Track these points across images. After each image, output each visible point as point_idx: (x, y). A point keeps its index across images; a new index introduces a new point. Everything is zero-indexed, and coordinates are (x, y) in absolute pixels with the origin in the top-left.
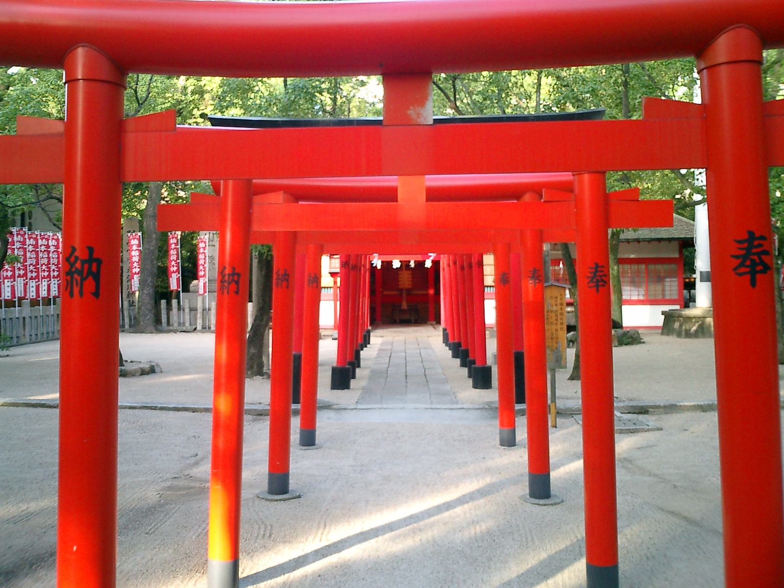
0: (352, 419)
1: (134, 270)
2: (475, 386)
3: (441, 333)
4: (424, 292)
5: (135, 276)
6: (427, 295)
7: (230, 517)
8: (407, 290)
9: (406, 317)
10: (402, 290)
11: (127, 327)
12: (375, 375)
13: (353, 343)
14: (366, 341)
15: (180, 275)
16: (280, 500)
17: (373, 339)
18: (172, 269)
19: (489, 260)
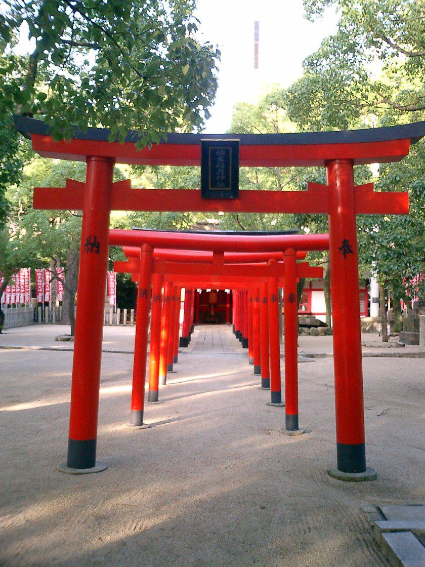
0: (190, 356)
1: (60, 289)
2: (244, 347)
3: (232, 328)
4: (223, 306)
5: (60, 292)
6: (226, 307)
7: (110, 383)
8: (214, 304)
9: (212, 320)
10: (211, 304)
11: (54, 321)
12: (197, 343)
13: (189, 331)
14: (192, 332)
15: (51, 293)
16: (381, 356)
17: (195, 331)
18: (39, 291)
19: (183, 291)
